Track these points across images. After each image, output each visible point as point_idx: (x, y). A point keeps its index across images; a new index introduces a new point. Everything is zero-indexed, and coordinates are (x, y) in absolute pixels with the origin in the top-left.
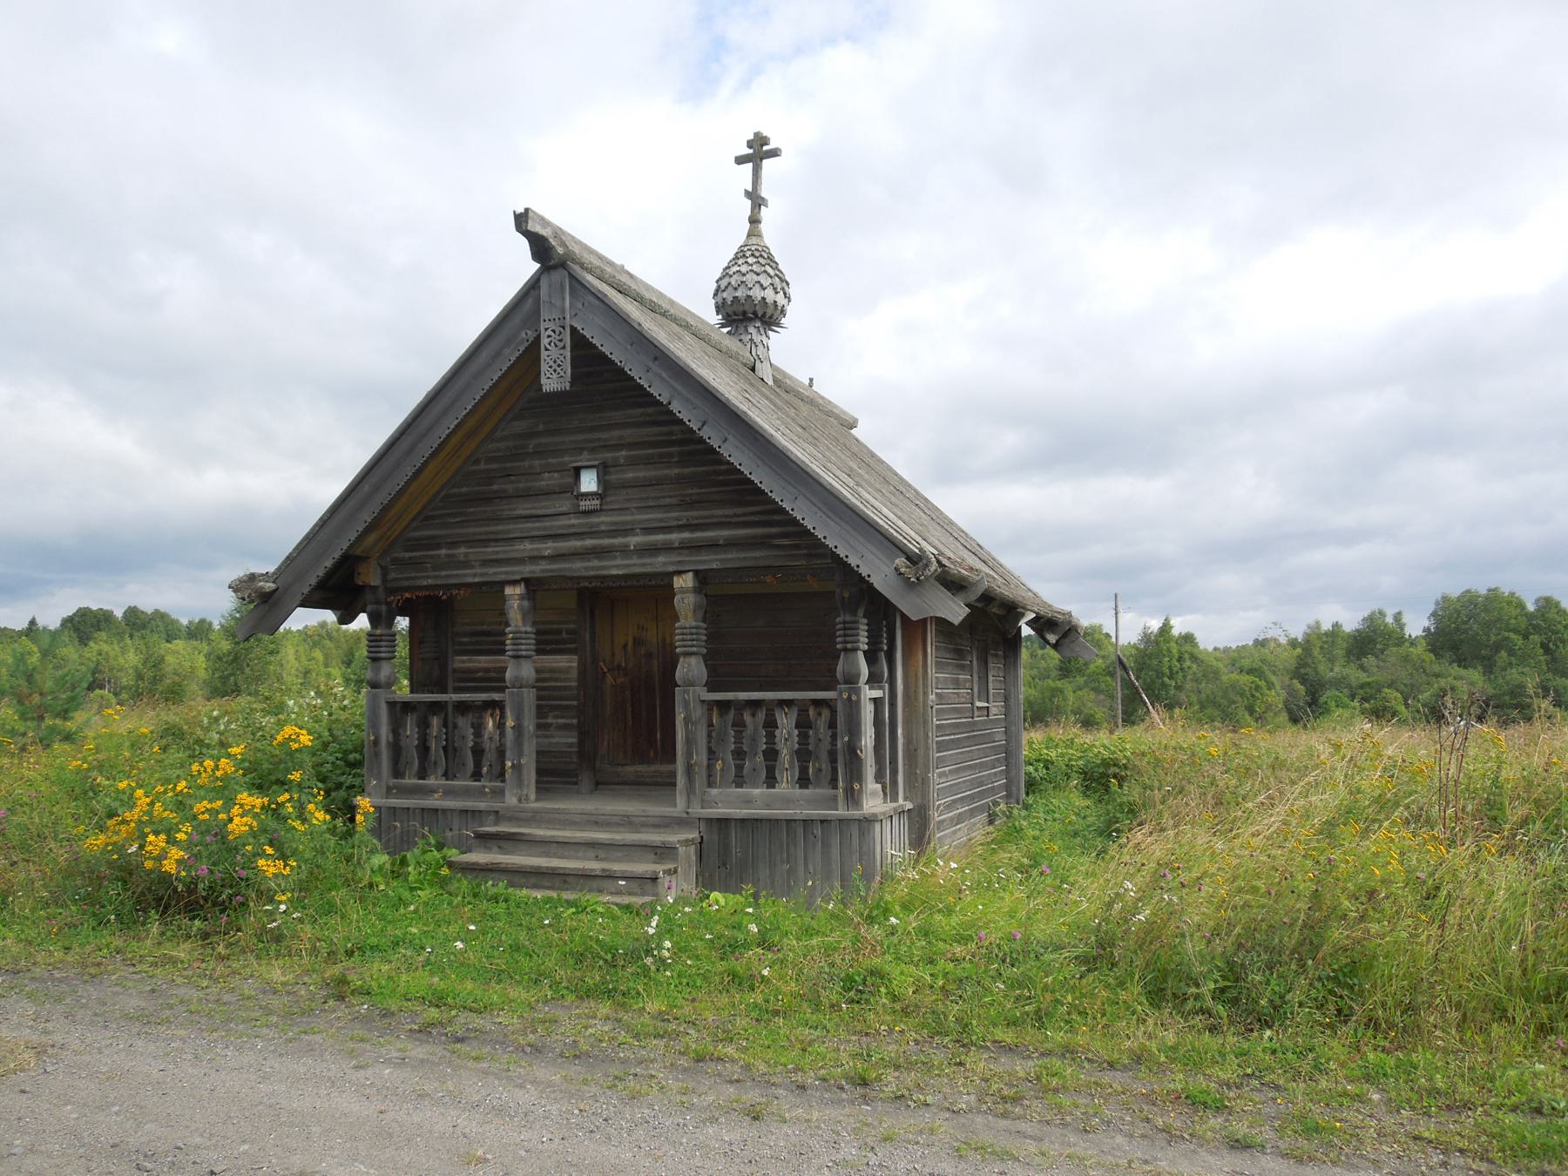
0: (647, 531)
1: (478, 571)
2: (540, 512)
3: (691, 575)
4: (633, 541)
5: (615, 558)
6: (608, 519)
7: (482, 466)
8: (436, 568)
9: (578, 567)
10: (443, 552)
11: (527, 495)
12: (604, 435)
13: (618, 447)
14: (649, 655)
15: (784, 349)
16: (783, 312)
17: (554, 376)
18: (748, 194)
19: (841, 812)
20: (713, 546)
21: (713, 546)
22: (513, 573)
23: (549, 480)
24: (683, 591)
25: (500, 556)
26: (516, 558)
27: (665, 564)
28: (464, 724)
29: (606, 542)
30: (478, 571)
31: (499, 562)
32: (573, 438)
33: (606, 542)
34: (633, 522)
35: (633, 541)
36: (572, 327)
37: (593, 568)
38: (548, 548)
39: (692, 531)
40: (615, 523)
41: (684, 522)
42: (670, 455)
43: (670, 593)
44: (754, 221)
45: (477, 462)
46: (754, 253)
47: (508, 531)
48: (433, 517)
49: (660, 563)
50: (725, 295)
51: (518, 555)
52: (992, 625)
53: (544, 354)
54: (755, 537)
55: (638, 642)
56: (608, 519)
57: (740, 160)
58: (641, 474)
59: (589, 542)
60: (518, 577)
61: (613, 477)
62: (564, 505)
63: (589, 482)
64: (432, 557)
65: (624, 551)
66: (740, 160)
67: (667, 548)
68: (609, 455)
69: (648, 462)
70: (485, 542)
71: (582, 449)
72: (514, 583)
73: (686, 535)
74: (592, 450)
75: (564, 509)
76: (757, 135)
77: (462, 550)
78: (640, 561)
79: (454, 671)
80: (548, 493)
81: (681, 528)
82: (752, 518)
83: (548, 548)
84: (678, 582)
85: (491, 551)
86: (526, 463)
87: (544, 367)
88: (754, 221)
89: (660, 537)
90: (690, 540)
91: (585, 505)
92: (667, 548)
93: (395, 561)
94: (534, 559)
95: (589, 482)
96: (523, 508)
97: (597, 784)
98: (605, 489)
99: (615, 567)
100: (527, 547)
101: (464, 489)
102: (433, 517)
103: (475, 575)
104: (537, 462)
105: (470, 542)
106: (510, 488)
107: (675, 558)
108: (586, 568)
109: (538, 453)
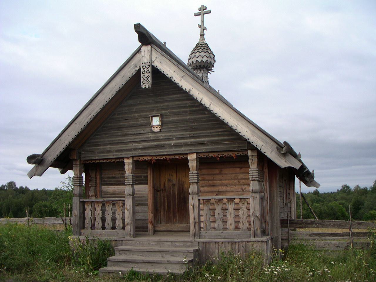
0: (178, 139)
1: (115, 154)
2: (138, 132)
4: (173, 142)
5: (166, 148)
6: (163, 135)
9: (152, 152)
10: (102, 147)
11: (131, 127)
14: (174, 185)
15: (214, 78)
16: (213, 66)
17: (146, 83)
18: (200, 26)
20: (202, 144)
21: (202, 144)
23: (140, 121)
24: (193, 160)
26: (127, 148)
27: (184, 150)
29: (163, 143)
30: (115, 154)
32: (150, 106)
33: (163, 143)
34: (173, 136)
35: (173, 142)
37: (158, 152)
38: (141, 145)
39: (195, 138)
41: (192, 135)
42: (186, 112)
43: (186, 161)
44: (202, 35)
46: (202, 47)
47: (125, 140)
49: (183, 150)
50: (193, 60)
51: (130, 148)
53: (142, 75)
56: (163, 135)
57: (196, 15)
58: (176, 118)
59: (156, 143)
60: (130, 156)
61: (165, 120)
62: (147, 130)
64: (98, 149)
65: (170, 146)
66: (196, 15)
67: (186, 145)
68: (163, 112)
70: (117, 144)
71: (154, 110)
72: (128, 158)
73: (193, 140)
74: (157, 110)
75: (146, 131)
76: (135, 25)
77: (109, 146)
78: (142, 152)
80: (141, 126)
81: (190, 137)
82: (222, 133)
83: (141, 145)
85: (119, 147)
86: (133, 115)
87: (142, 80)
88: (202, 35)
89: (183, 141)
90: (195, 142)
91: (154, 129)
92: (186, 145)
94: (135, 149)
95: (156, 121)
96: (131, 131)
98: (162, 124)
99: (166, 151)
100: (133, 145)
104: (136, 115)
106: (126, 124)
108: (155, 152)
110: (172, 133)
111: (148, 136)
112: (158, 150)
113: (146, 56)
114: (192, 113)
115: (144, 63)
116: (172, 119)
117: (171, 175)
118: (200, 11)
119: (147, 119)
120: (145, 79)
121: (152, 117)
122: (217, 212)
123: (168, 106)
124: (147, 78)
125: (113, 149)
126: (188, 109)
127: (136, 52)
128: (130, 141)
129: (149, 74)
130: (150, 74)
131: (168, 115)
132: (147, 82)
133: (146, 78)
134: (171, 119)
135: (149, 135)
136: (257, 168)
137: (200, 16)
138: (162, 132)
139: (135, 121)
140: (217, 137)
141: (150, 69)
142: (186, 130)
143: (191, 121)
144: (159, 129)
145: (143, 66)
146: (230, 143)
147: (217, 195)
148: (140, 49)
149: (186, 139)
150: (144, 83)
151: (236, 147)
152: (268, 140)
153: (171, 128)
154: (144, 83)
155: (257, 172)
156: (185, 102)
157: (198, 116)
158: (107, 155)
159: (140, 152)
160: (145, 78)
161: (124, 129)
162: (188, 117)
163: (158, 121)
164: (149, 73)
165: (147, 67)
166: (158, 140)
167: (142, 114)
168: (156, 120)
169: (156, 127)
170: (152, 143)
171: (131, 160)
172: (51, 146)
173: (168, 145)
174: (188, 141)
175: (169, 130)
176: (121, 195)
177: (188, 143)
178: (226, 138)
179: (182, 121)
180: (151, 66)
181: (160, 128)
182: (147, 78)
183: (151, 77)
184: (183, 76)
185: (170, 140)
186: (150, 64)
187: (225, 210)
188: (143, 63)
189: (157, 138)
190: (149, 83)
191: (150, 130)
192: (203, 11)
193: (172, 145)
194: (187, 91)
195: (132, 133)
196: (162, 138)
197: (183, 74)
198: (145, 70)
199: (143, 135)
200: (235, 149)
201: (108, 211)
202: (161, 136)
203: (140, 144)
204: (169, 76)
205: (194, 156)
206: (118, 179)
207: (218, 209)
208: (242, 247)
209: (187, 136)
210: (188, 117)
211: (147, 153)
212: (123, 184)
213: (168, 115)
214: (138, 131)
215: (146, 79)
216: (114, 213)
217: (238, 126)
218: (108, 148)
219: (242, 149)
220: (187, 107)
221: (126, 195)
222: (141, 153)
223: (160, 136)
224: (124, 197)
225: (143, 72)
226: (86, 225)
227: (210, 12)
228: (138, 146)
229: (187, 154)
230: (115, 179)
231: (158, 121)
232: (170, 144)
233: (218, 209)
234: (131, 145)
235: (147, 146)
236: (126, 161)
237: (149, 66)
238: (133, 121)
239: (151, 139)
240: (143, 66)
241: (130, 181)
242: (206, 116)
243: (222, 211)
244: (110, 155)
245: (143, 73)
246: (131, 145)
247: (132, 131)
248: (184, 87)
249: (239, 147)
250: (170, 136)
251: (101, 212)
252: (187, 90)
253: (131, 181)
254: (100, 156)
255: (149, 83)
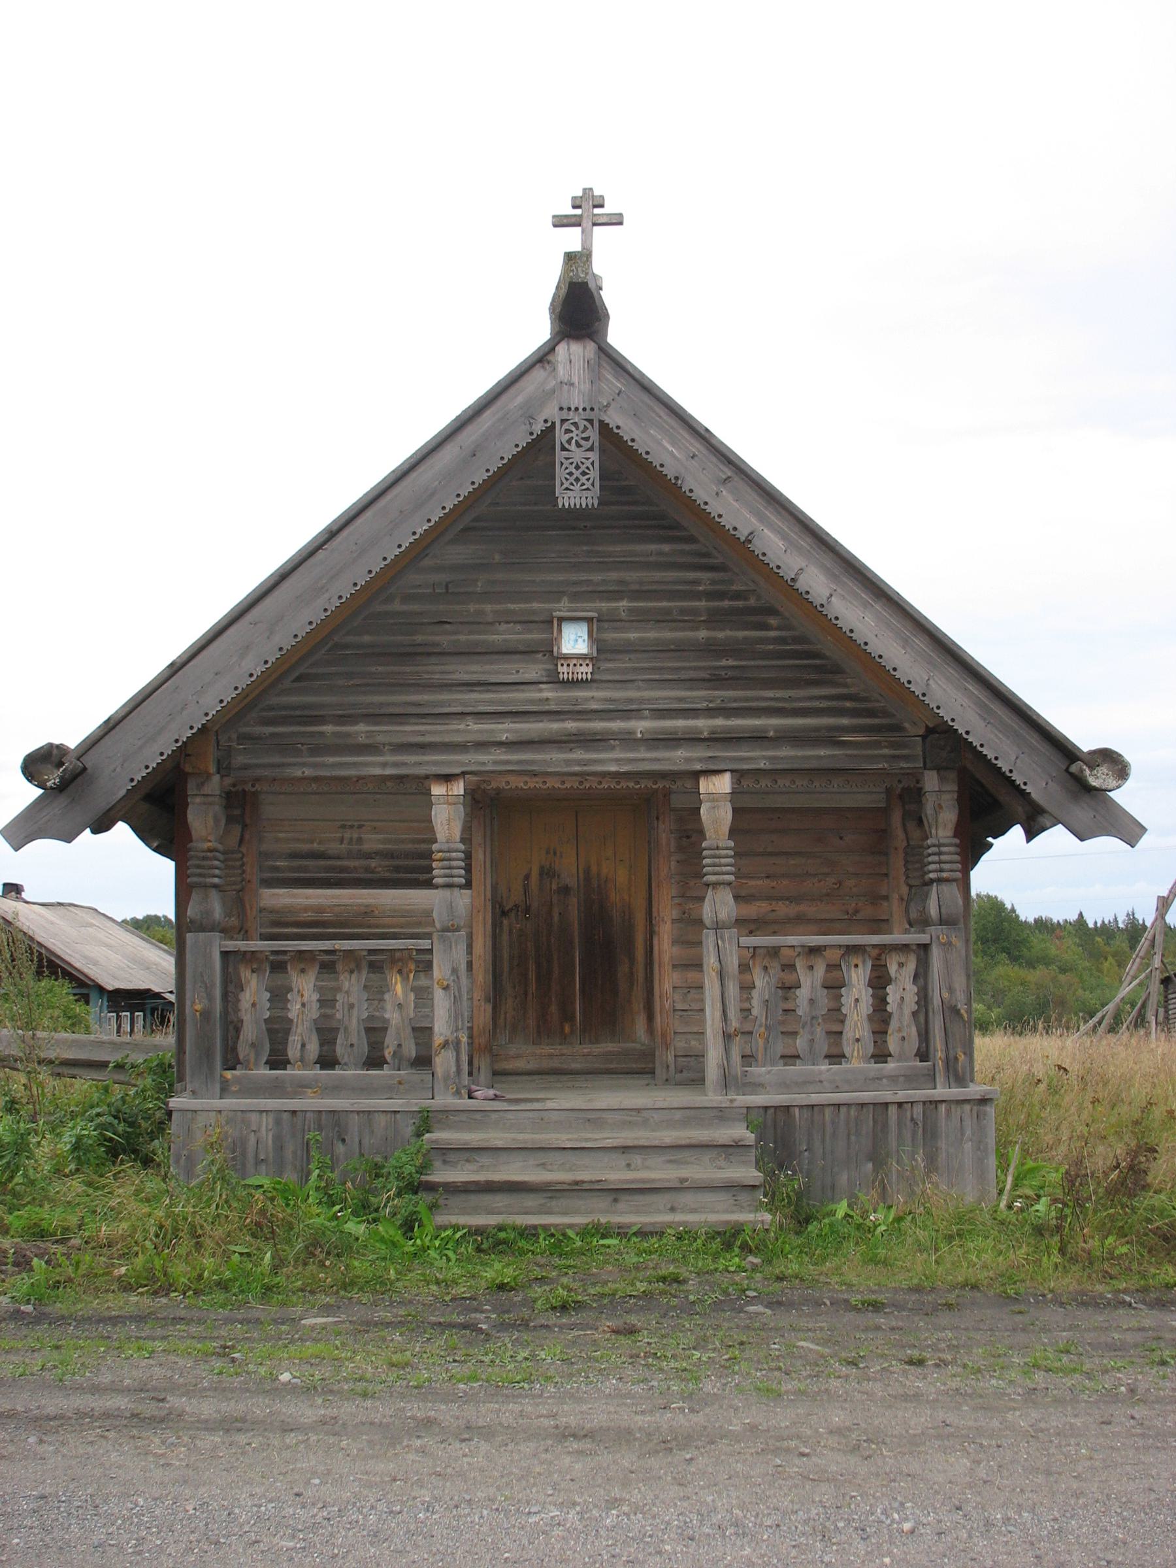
3: (727, 776)
4: (641, 726)
5: (613, 748)
7: (397, 606)
8: (316, 750)
9: (554, 759)
10: (328, 729)
12: (597, 577)
13: (616, 595)
14: (565, 890)
17: (577, 490)
19: (941, 1091)
20: (758, 738)
21: (758, 738)
22: (449, 763)
24: (714, 798)
25: (428, 739)
28: (352, 985)
29: (598, 725)
31: (422, 747)
33: (598, 725)
34: (642, 701)
35: (641, 726)
36: (600, 421)
37: (579, 762)
38: (505, 730)
39: (728, 717)
40: (611, 700)
42: (694, 612)
45: (389, 599)
47: (442, 704)
48: (316, 677)
49: (678, 758)
52: (494, 888)
53: (560, 455)
54: (817, 729)
55: (547, 873)
57: (561, 222)
58: (652, 635)
59: (571, 725)
62: (533, 671)
63: (574, 640)
64: (312, 734)
65: (628, 740)
66: (561, 222)
67: (693, 739)
69: (663, 619)
71: (563, 593)
73: (719, 722)
74: (575, 597)
77: (361, 727)
78: (649, 755)
79: (262, 910)
81: (710, 712)
82: (834, 704)
83: (505, 730)
84: (707, 786)
85: (410, 731)
86: (472, 607)
89: (680, 723)
91: (564, 671)
92: (693, 739)
93: (243, 738)
94: (481, 746)
95: (574, 640)
97: (495, 1073)
100: (475, 729)
101: (367, 638)
102: (316, 677)
103: (384, 765)
104: (488, 608)
105: (373, 717)
106: (444, 640)
107: (701, 752)
108: (568, 762)
109: (486, 596)
110: (639, 689)
111: (537, 695)
112: (579, 755)
113: (575, 380)
114: (715, 619)
115: (569, 409)
116: (637, 635)
117: (555, 853)
118: (578, 212)
119: (532, 626)
120: (574, 471)
121: (561, 620)
122: (803, 993)
123: (621, 582)
124: (583, 468)
125: (380, 739)
126: (702, 604)
127: (530, 362)
128: (459, 709)
129: (589, 454)
130: (594, 456)
131: (621, 621)
132: (583, 484)
133: (577, 468)
134: (633, 636)
135: (541, 690)
136: (955, 836)
137: (579, 229)
138: (595, 685)
139: (480, 633)
140: (829, 716)
141: (594, 434)
142: (692, 683)
143: (712, 649)
144: (585, 671)
145: (563, 421)
146: (866, 743)
147: (751, 932)
148: (553, 349)
149: (693, 718)
150: (567, 489)
151: (884, 756)
152: (1033, 739)
153: (635, 669)
154: (567, 489)
155: (958, 850)
156: (691, 575)
157: (741, 634)
158: (355, 764)
159: (504, 757)
160: (572, 469)
161: (433, 660)
162: (702, 634)
163: (580, 640)
164: (591, 449)
165: (581, 428)
166: (579, 712)
167: (512, 606)
168: (573, 637)
169: (574, 661)
170: (555, 726)
171: (459, 788)
172: (130, 712)
173: (619, 737)
174: (703, 724)
175: (629, 677)
176: (417, 924)
177: (701, 733)
178: (845, 721)
179: (679, 649)
180: (596, 424)
181: (590, 669)
182: (583, 468)
183: (597, 465)
184: (724, 477)
185: (629, 719)
186: (588, 414)
187: (835, 986)
188: (565, 406)
189: (578, 708)
190: (588, 489)
191: (544, 673)
192: (587, 212)
193: (639, 736)
194: (743, 539)
195: (466, 678)
196: (594, 706)
197: (726, 469)
198: (576, 432)
199: (517, 690)
200: (881, 766)
201: (347, 992)
202: (594, 697)
203: (500, 726)
204: (670, 472)
205: (723, 784)
206: (339, 863)
207: (810, 982)
208: (912, 1119)
209: (699, 706)
210: (702, 634)
211: (533, 762)
212: (428, 884)
213: (621, 621)
214: (497, 673)
215: (577, 474)
216: (326, 1002)
217: (931, 682)
218: (357, 733)
219: (905, 766)
220: (697, 596)
221: (438, 925)
222: (507, 762)
223: (587, 700)
224: (428, 936)
225: (567, 446)
226: (243, 1051)
227: (617, 220)
228: (492, 731)
229: (696, 775)
230: (322, 863)
231: (580, 640)
232: (631, 732)
233: (810, 982)
234: (462, 727)
235: (534, 736)
236: (437, 790)
237: (591, 421)
238: (470, 633)
239: (553, 707)
240: (563, 421)
241: (456, 872)
242: (772, 634)
243: (826, 991)
244: (366, 764)
245: (563, 449)
246: (462, 727)
247: (467, 673)
248: (727, 522)
249: (894, 757)
250: (630, 701)
251: (315, 997)
252: (742, 534)
253: (435, 872)
254: (405, 764)
255: (588, 489)
